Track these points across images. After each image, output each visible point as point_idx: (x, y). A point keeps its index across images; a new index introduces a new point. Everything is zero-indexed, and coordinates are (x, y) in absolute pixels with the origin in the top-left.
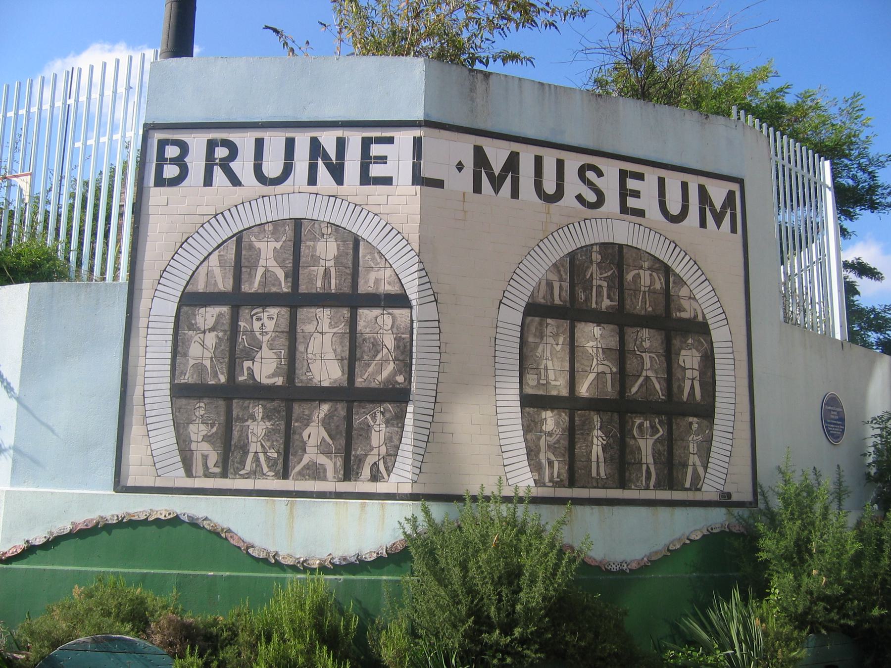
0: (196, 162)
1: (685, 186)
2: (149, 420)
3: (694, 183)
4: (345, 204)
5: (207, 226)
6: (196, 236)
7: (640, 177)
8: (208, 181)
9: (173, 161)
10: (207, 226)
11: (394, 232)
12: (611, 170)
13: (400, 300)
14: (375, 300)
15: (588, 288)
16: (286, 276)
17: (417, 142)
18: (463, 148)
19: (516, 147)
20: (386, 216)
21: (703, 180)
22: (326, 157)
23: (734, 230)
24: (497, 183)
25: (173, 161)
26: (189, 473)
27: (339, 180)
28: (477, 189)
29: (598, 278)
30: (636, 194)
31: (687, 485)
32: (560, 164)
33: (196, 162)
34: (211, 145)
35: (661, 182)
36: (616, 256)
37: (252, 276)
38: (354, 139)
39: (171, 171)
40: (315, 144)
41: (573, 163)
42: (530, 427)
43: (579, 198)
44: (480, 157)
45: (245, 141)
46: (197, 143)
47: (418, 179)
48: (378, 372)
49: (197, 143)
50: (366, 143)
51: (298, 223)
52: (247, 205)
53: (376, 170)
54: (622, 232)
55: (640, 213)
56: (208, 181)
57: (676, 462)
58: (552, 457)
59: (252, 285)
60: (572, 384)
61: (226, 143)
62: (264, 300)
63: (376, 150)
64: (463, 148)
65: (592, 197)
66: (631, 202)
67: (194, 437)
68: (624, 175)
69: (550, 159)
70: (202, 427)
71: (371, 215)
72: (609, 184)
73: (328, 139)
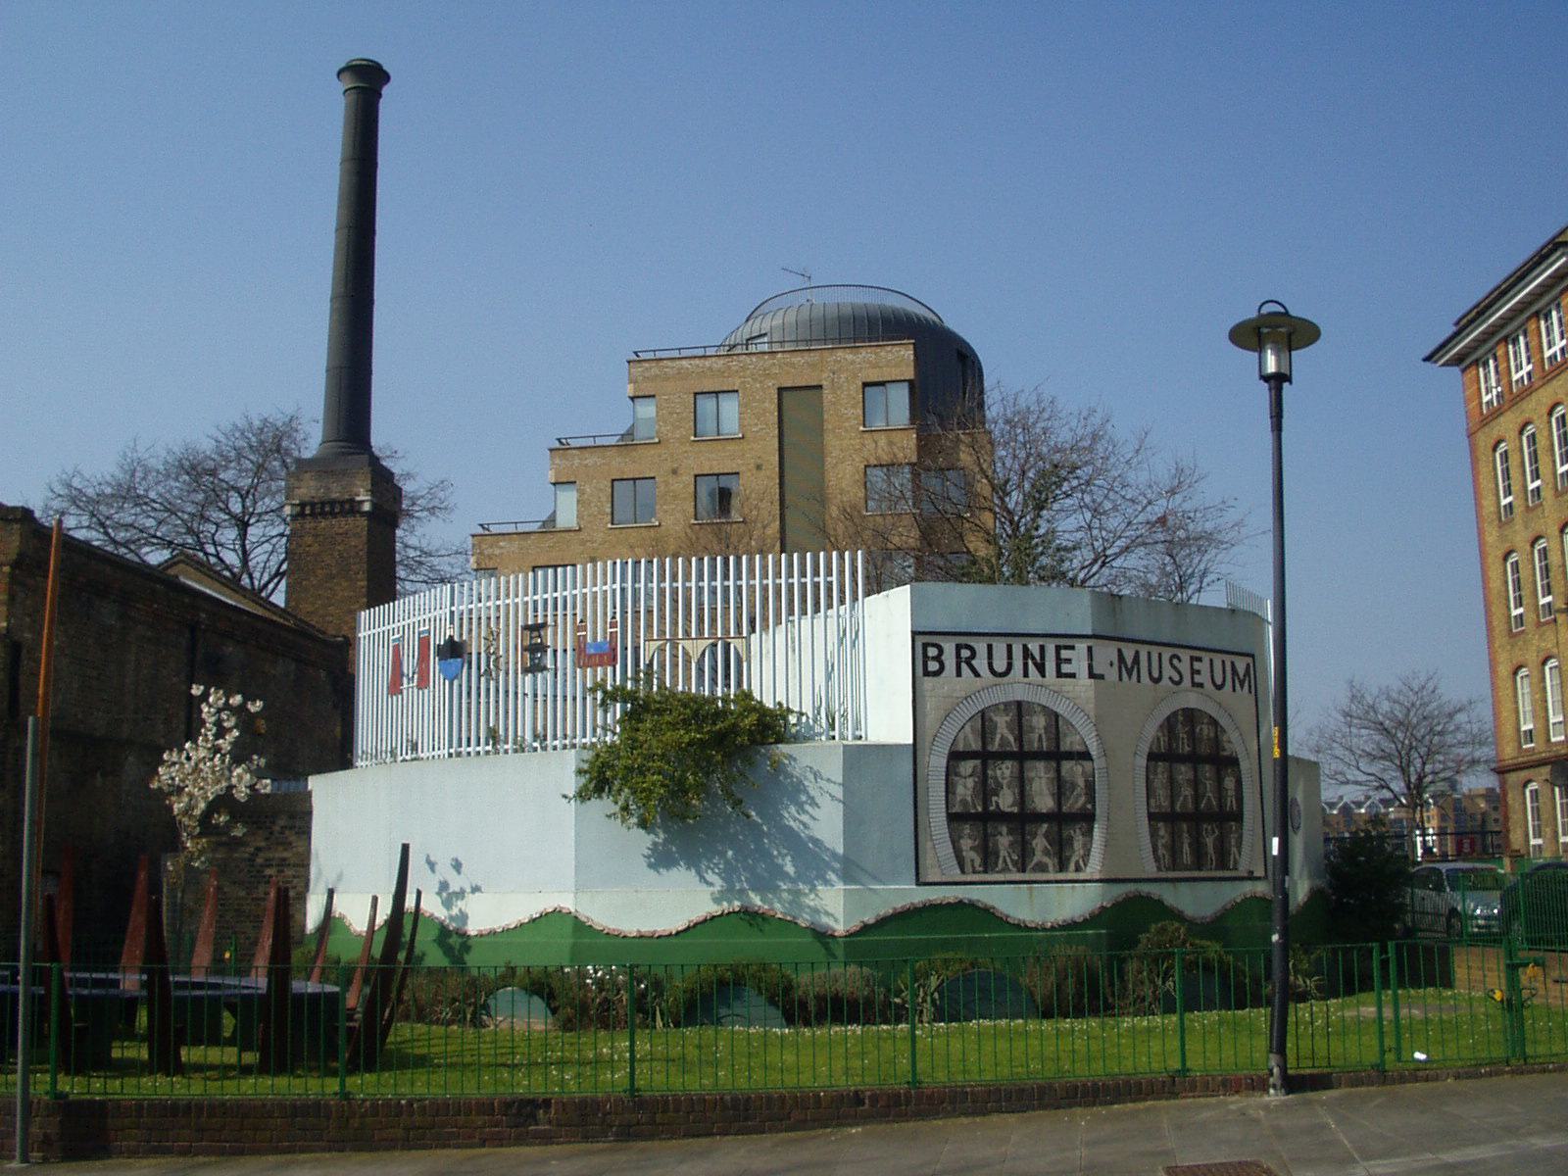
7: (1199, 659)
8: (959, 674)
9: (934, 658)
13: (1086, 756)
14: (1070, 756)
17: (1090, 649)
20: (1074, 697)
21: (1024, 640)
22: (1033, 658)
25: (934, 658)
26: (963, 872)
29: (1182, 732)
34: (959, 648)
36: (1190, 716)
39: (933, 666)
40: (1025, 648)
45: (981, 647)
47: (1092, 675)
48: (1076, 802)
49: (949, 647)
50: (1058, 649)
53: (1066, 668)
55: (1201, 685)
56: (959, 674)
59: (995, 747)
60: (1173, 804)
63: (1064, 654)
67: (964, 848)
69: (1155, 651)
70: (969, 841)
72: (1184, 667)
73: (1034, 646)
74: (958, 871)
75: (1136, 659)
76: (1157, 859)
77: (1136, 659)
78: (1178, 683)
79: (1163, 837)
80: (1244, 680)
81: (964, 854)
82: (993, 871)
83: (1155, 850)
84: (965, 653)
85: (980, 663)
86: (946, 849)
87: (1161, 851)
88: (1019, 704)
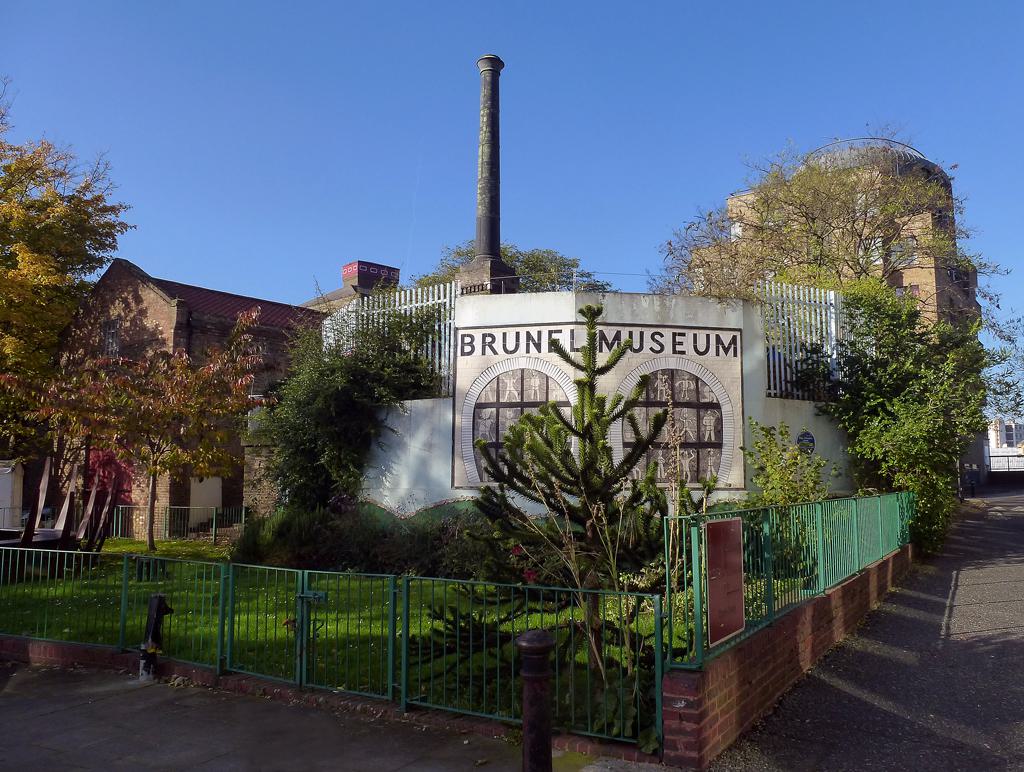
0: (478, 344)
12: (668, 333)
15: (655, 390)
19: (619, 328)
21: (718, 332)
22: (533, 340)
23: (735, 355)
24: (726, 350)
33: (478, 344)
34: (484, 336)
37: (504, 395)
38: (545, 331)
39: (468, 349)
40: (528, 333)
41: (648, 333)
43: (651, 349)
45: (498, 334)
46: (478, 335)
51: (523, 370)
53: (678, 348)
54: (670, 362)
57: (701, 469)
59: (504, 399)
60: (637, 432)
61: (469, 336)
62: (510, 405)
63: (678, 339)
65: (658, 348)
66: (678, 348)
72: (667, 339)
73: (534, 332)
80: (729, 348)
84: (489, 339)
85: (498, 345)
88: (672, 370)
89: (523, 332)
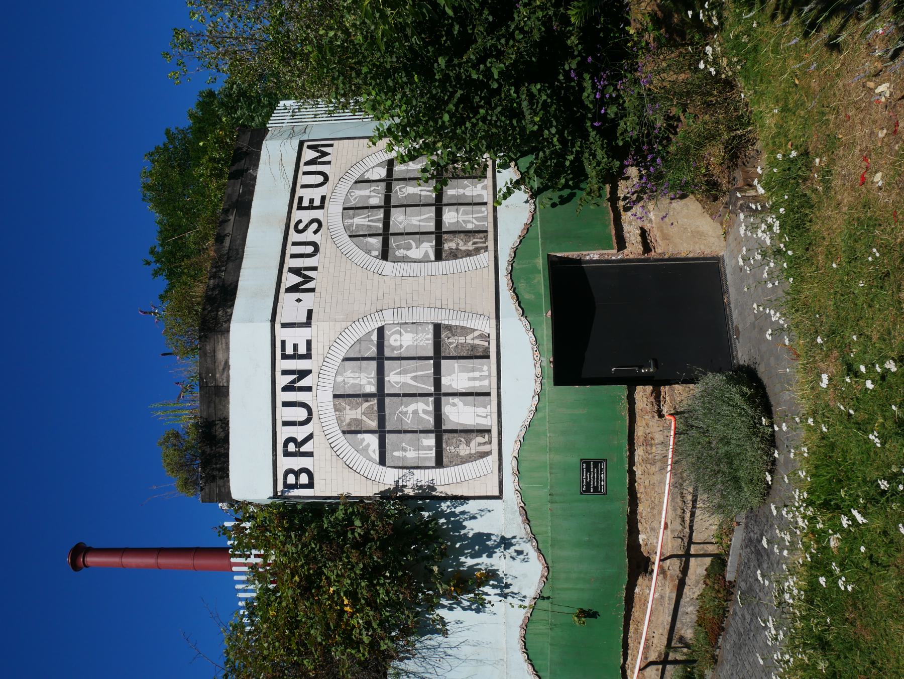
1: (305, 173)
2: (459, 481)
3: (304, 168)
4: (323, 368)
5: (338, 453)
6: (345, 459)
7: (301, 199)
8: (310, 454)
9: (297, 478)
10: (338, 453)
11: (340, 337)
12: (297, 215)
16: (367, 401)
17: (284, 325)
18: (287, 299)
21: (302, 163)
22: (294, 381)
23: (332, 145)
24: (308, 279)
25: (297, 478)
26: (488, 454)
27: (308, 372)
28: (312, 290)
30: (312, 201)
31: (486, 344)
32: (295, 244)
34: (287, 454)
35: (303, 186)
38: (282, 364)
39: (304, 479)
40: (285, 389)
41: (294, 236)
42: (455, 255)
43: (315, 232)
44: (289, 290)
45: (284, 433)
46: (285, 463)
47: (308, 324)
49: (285, 463)
50: (285, 357)
51: (335, 396)
52: (325, 429)
53: (302, 350)
54: (334, 209)
55: (323, 198)
56: (310, 454)
58: (471, 243)
61: (286, 445)
63: (289, 351)
64: (287, 299)
65: (315, 226)
67: (467, 452)
68: (300, 208)
69: (291, 250)
70: (461, 447)
71: (330, 351)
72: (306, 216)
74: (489, 458)
75: (296, 271)
76: (477, 251)
77: (296, 271)
78: (319, 222)
79: (458, 244)
80: (321, 152)
81: (473, 452)
82: (487, 349)
83: (468, 254)
86: (468, 469)
87: (470, 246)
89: (282, 396)
